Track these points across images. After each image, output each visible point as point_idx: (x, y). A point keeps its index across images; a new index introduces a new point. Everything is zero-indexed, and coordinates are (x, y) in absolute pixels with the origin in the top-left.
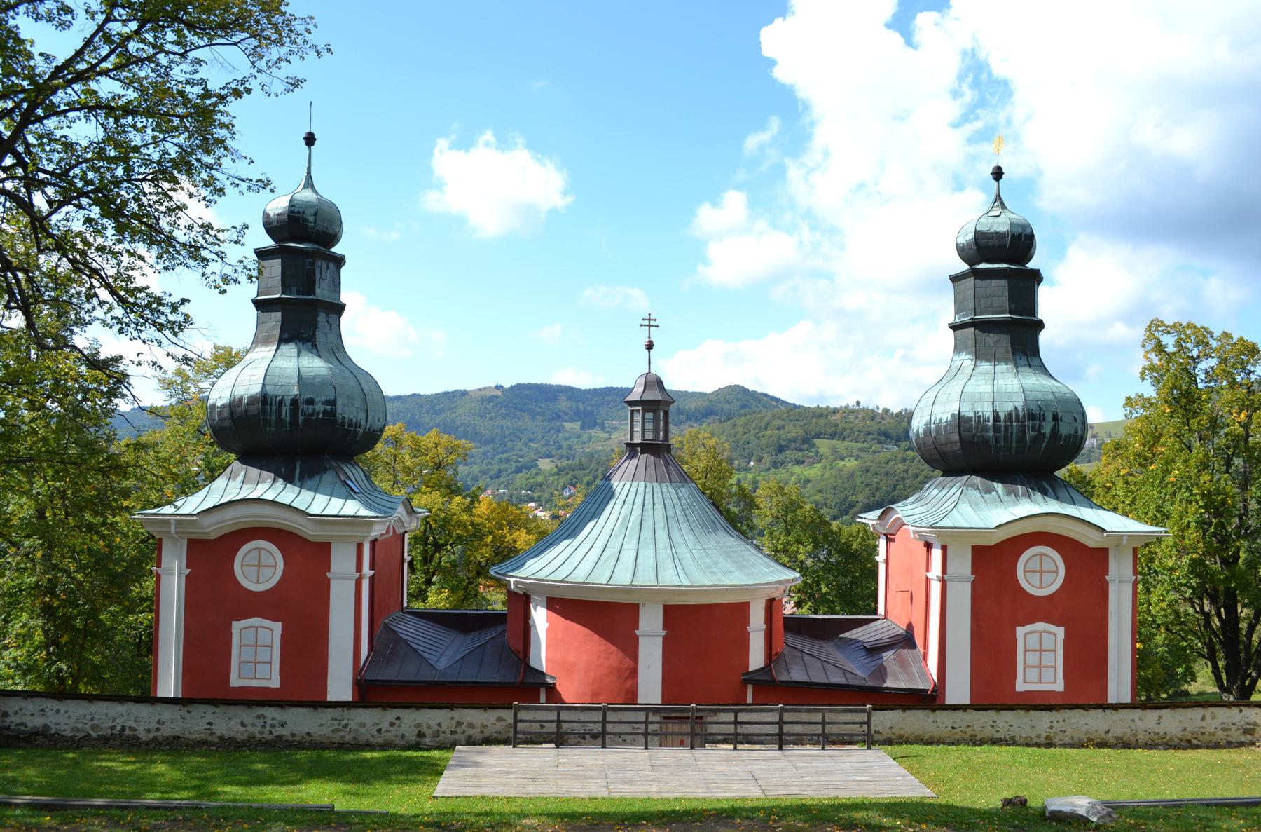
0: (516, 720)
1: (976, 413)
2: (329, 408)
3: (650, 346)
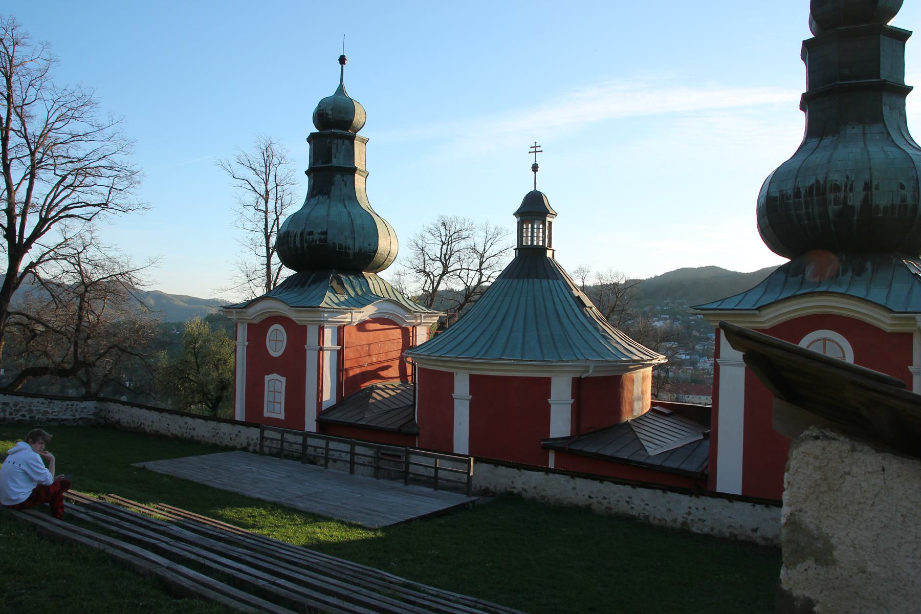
0: (262, 438)
1: (781, 191)
2: (323, 237)
3: (535, 168)
